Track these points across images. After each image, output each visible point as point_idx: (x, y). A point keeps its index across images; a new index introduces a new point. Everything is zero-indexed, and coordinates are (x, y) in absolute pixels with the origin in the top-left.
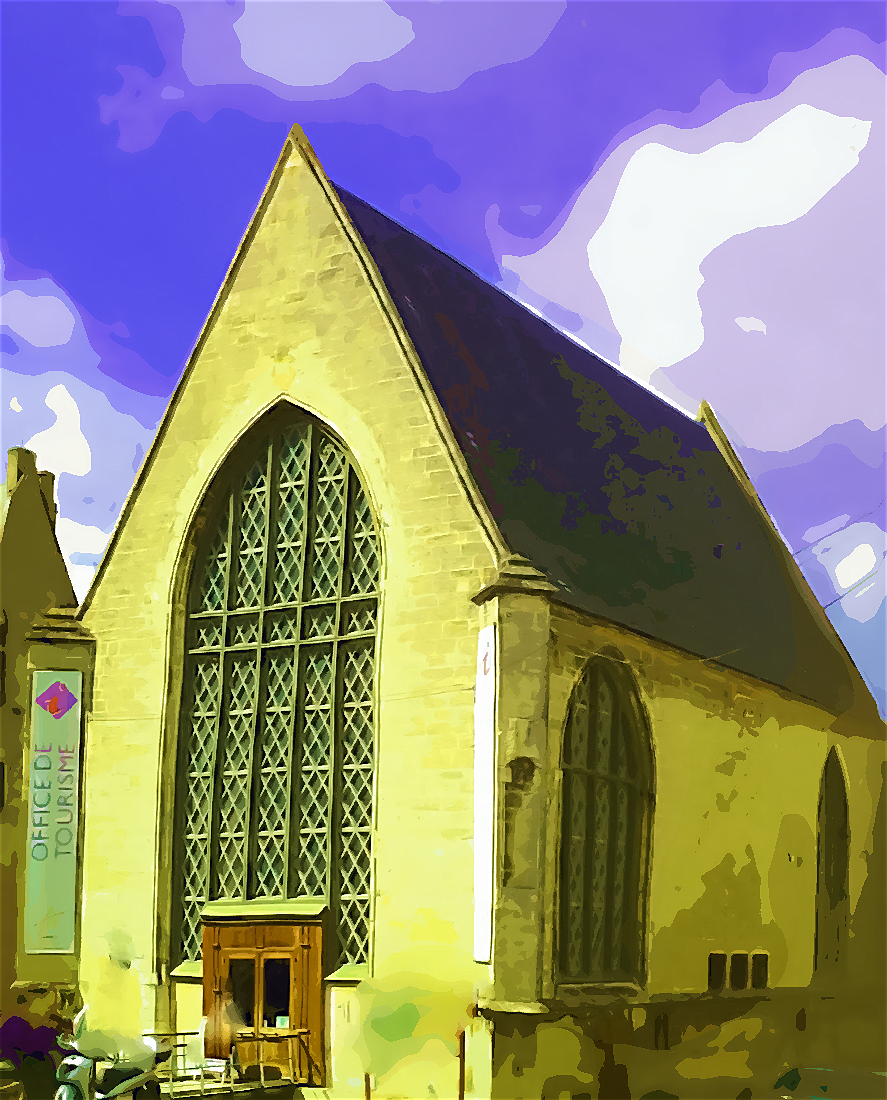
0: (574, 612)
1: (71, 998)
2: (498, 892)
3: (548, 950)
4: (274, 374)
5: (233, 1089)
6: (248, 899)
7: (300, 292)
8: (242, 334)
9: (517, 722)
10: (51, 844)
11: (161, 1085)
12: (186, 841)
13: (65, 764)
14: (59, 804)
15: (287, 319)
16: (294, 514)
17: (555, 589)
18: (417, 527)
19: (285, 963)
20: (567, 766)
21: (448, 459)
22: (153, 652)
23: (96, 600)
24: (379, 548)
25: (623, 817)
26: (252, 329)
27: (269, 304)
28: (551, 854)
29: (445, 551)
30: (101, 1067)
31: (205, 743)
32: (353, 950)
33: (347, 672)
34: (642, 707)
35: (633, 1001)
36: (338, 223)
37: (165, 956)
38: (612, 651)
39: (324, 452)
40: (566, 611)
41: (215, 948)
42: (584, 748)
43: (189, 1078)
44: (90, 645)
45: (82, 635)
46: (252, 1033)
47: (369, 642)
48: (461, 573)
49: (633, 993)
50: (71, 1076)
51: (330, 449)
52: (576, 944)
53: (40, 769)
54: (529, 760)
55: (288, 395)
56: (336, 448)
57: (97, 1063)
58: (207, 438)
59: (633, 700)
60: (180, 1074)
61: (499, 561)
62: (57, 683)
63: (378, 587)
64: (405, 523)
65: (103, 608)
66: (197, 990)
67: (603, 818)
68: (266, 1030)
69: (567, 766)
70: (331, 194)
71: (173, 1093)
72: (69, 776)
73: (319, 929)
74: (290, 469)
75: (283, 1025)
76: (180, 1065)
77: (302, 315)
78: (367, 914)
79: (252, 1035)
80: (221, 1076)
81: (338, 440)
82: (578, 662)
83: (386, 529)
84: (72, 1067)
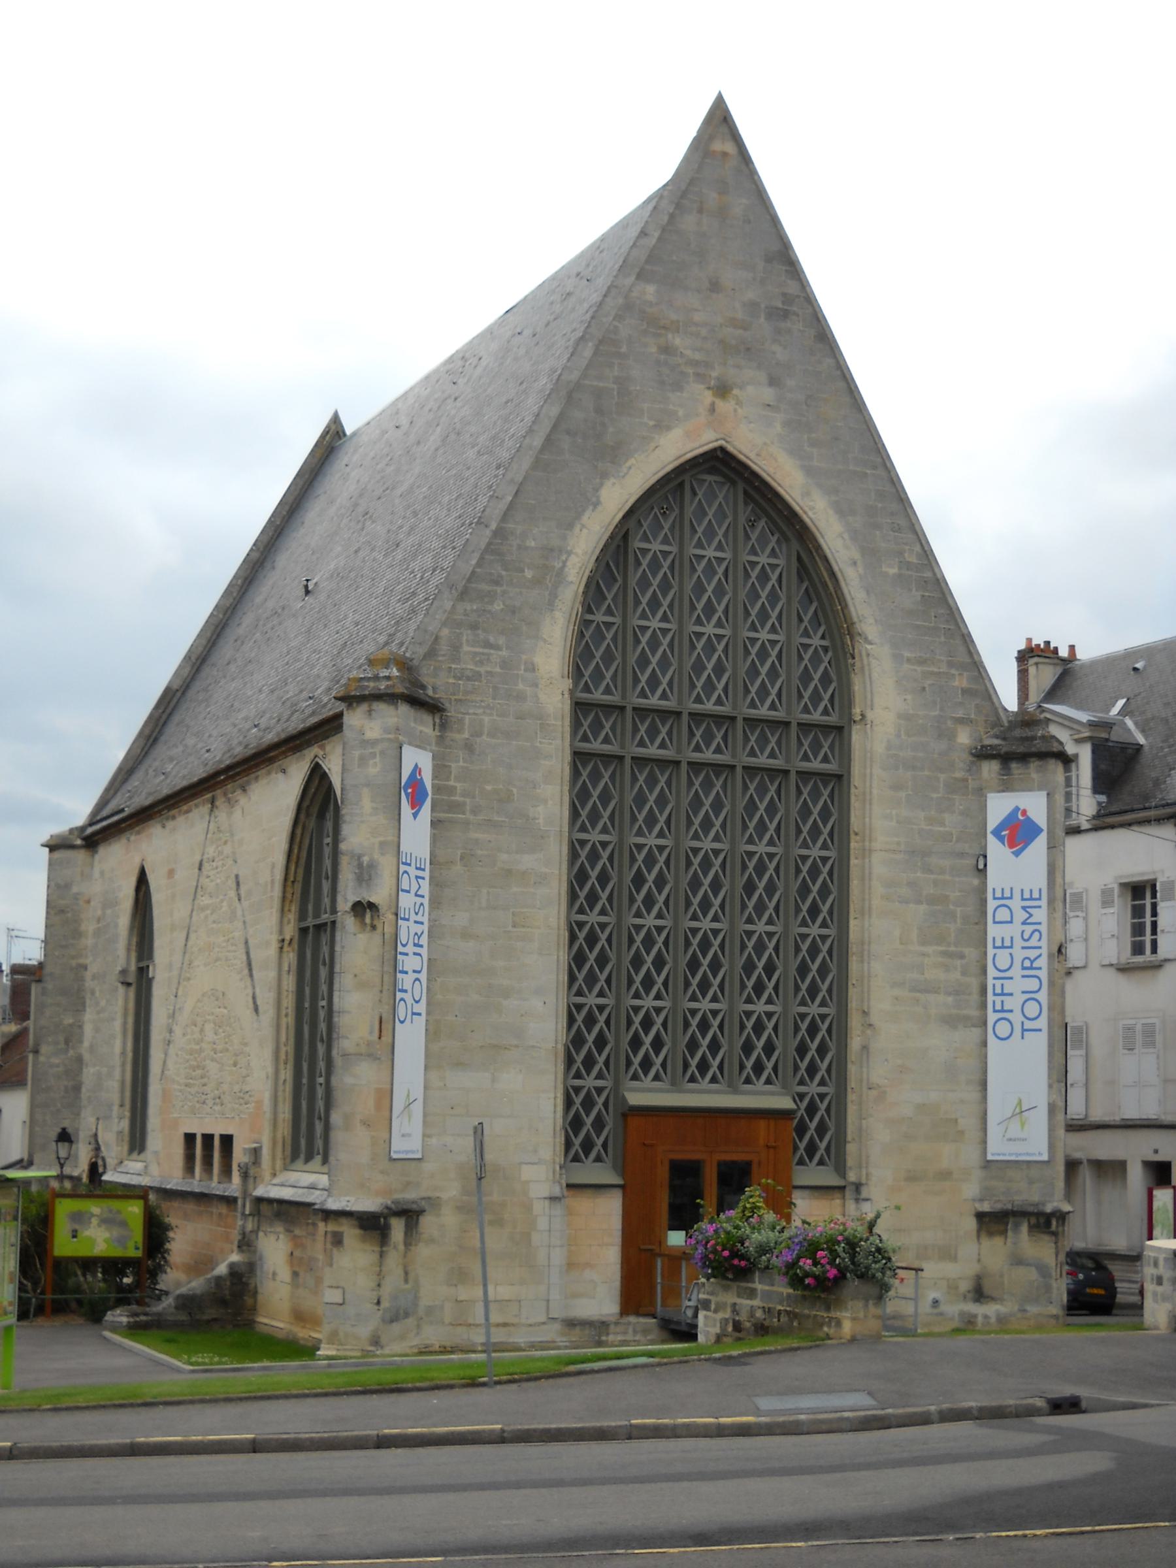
10: (1016, 1017)
13: (1031, 915)
14: (1024, 968)
18: (907, 654)
48: (961, 721)
62: (1017, 809)
72: (1036, 930)
77: (748, 351)
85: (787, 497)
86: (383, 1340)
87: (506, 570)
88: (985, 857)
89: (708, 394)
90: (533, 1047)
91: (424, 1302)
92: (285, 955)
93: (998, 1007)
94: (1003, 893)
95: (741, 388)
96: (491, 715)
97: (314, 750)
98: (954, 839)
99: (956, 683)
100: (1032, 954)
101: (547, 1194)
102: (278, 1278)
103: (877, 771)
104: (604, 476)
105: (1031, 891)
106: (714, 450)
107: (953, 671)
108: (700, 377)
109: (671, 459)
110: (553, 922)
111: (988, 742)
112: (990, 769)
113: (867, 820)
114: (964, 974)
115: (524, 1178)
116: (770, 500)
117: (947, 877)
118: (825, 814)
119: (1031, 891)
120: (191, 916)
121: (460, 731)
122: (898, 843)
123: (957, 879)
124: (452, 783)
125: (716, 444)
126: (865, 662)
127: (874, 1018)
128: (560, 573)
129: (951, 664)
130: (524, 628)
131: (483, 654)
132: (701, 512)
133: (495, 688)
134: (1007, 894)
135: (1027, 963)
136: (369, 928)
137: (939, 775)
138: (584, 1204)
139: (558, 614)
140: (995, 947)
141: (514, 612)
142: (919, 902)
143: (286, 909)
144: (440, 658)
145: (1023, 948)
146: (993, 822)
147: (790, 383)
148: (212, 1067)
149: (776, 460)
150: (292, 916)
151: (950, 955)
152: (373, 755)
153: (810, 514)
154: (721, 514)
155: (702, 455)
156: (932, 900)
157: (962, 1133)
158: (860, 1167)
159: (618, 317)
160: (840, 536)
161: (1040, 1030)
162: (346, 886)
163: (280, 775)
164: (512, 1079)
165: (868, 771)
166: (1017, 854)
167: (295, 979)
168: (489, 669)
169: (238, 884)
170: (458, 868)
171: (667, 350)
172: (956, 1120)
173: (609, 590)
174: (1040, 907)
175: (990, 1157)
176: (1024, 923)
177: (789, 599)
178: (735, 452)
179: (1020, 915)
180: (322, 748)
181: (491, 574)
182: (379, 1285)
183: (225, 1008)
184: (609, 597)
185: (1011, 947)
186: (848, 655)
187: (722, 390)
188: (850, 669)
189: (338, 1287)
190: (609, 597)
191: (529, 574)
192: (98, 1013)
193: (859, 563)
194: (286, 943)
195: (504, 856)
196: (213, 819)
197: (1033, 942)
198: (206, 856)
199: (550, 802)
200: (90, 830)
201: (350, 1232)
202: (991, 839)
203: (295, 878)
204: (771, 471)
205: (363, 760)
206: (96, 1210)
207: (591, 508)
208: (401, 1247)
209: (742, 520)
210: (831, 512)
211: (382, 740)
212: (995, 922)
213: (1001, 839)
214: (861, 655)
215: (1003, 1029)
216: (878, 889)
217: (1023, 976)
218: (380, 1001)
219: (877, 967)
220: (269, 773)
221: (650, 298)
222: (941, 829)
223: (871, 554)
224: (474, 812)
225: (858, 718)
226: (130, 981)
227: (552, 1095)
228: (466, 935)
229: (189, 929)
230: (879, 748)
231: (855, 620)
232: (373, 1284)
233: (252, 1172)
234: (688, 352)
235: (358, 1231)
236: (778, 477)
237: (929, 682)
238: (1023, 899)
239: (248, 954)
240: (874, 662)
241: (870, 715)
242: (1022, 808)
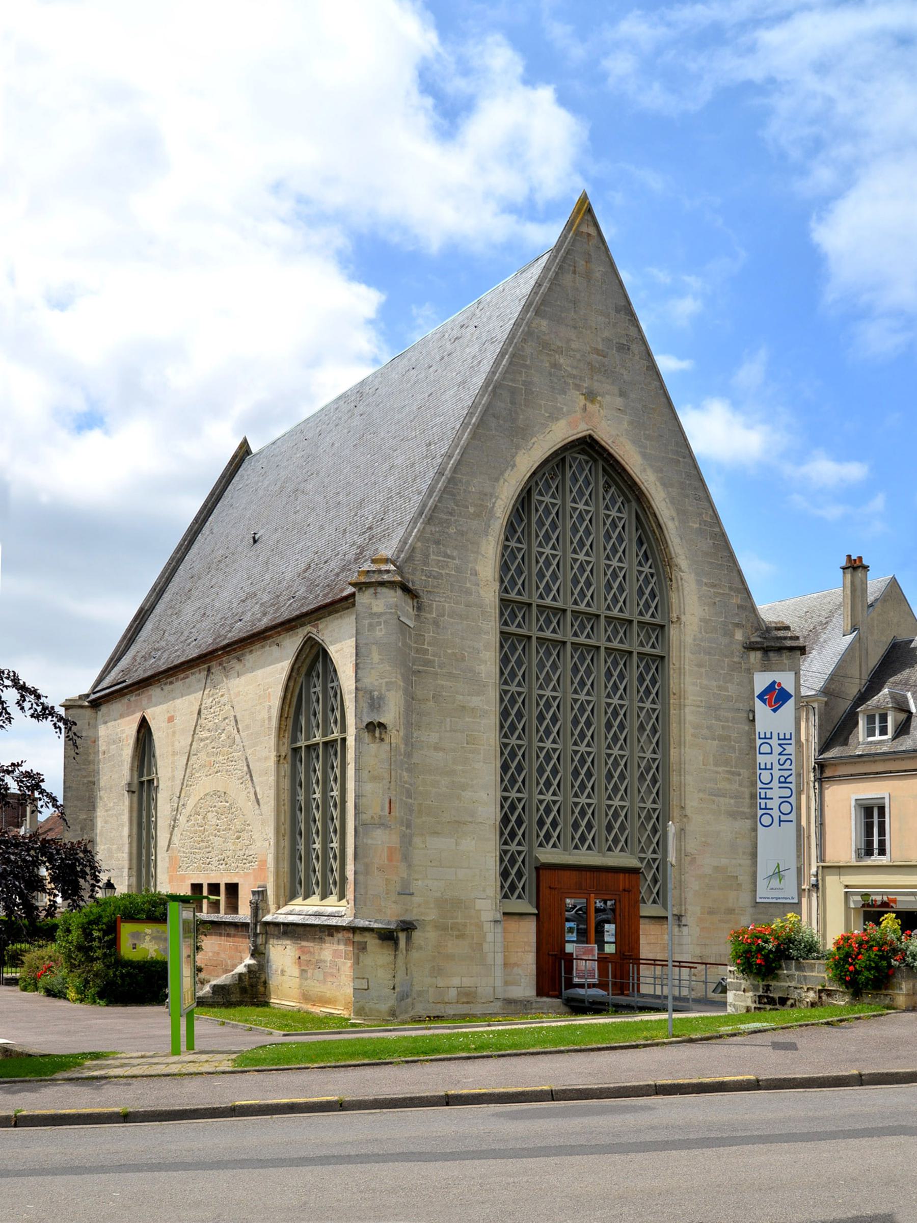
10: (775, 813)
14: (780, 782)
18: (705, 580)
48: (737, 625)
62: (774, 682)
85: (631, 472)
86: (397, 1013)
87: (457, 506)
88: (754, 712)
89: (582, 397)
90: (481, 823)
91: (417, 988)
92: (281, 766)
93: (763, 806)
96: (450, 603)
97: (308, 628)
99: (734, 601)
100: (786, 773)
101: (492, 919)
102: (288, 973)
103: (688, 654)
104: (518, 448)
106: (585, 437)
107: (732, 593)
108: (577, 387)
109: (560, 440)
110: (492, 742)
111: (753, 640)
112: (755, 657)
113: (682, 685)
114: (740, 785)
115: (477, 908)
116: (619, 474)
117: (730, 724)
118: (654, 681)
120: (191, 745)
122: (701, 701)
123: (736, 726)
124: (426, 647)
125: (587, 433)
126: (680, 583)
127: (688, 812)
128: (491, 511)
129: (731, 588)
130: (470, 546)
131: (443, 561)
132: (575, 479)
134: (768, 736)
135: (782, 779)
136: (378, 740)
138: (513, 925)
140: (760, 769)
141: (462, 535)
142: (715, 739)
143: (281, 736)
144: (416, 562)
145: (780, 770)
146: (758, 690)
148: (217, 841)
149: (624, 446)
150: (286, 740)
151: (733, 773)
152: (379, 623)
153: (645, 484)
154: (587, 483)
155: (578, 439)
156: (721, 738)
157: (739, 885)
158: (681, 905)
159: (524, 340)
160: (664, 500)
161: (792, 821)
162: (362, 711)
163: (275, 648)
164: (468, 844)
165: (682, 654)
167: (289, 781)
168: (447, 572)
169: (236, 721)
170: (431, 704)
171: (555, 365)
173: (519, 526)
174: (791, 744)
175: (758, 900)
176: (780, 754)
177: (630, 540)
178: (599, 439)
180: (316, 626)
181: (447, 508)
182: (394, 977)
183: (227, 802)
184: (519, 531)
185: (771, 769)
186: (668, 579)
187: (591, 396)
188: (669, 588)
189: (363, 978)
190: (519, 531)
192: (107, 811)
193: (676, 519)
194: (282, 758)
196: (209, 681)
197: (787, 766)
198: (204, 705)
199: (489, 663)
200: (93, 697)
201: (372, 942)
202: (757, 701)
203: (288, 715)
204: (621, 453)
205: (371, 626)
206: (148, 931)
207: (510, 468)
208: (404, 952)
209: (601, 483)
210: (658, 484)
211: (385, 613)
212: (760, 753)
213: (764, 701)
214: (677, 580)
215: (766, 820)
216: (689, 730)
217: (780, 788)
218: (389, 789)
219: (689, 779)
220: (263, 647)
221: (543, 329)
223: (682, 514)
224: (440, 667)
225: (675, 620)
226: (133, 790)
228: (437, 748)
229: (189, 753)
230: (689, 640)
231: (674, 556)
232: (390, 976)
233: (261, 905)
234: (569, 369)
235: (377, 941)
236: (625, 458)
237: (718, 599)
238: (779, 739)
239: (248, 766)
240: (686, 585)
241: (683, 618)
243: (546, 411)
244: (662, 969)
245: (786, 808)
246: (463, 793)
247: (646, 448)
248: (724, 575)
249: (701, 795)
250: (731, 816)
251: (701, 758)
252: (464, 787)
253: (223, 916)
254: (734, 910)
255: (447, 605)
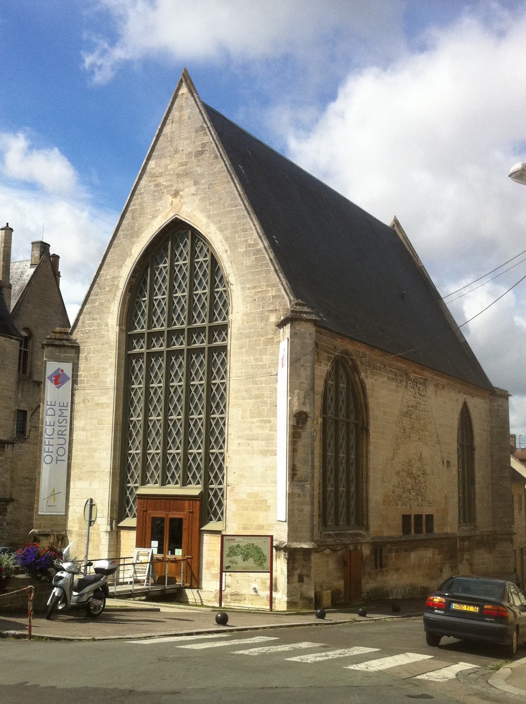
0: (328, 331)
1: (63, 540)
2: (289, 484)
3: (316, 513)
4: (172, 204)
5: (150, 589)
6: (162, 486)
7: (186, 162)
8: (156, 183)
9: (298, 392)
10: (54, 455)
11: (109, 588)
12: (128, 455)
13: (63, 413)
14: (58, 435)
15: (178, 175)
16: (182, 278)
17: (318, 318)
19: (181, 520)
20: (325, 416)
21: (264, 250)
22: (109, 353)
23: (80, 323)
24: (228, 297)
25: (353, 442)
26: (161, 180)
27: (169, 168)
28: (317, 463)
29: (263, 299)
30: (76, 577)
31: (138, 402)
32: (215, 514)
33: (211, 364)
34: (362, 382)
35: (362, 540)
36: (205, 126)
37: (115, 516)
38: (347, 353)
39: (198, 246)
40: (323, 331)
41: (144, 511)
42: (333, 405)
43: (126, 583)
44: (76, 348)
45: (72, 343)
46: (162, 557)
47: (224, 348)
48: (271, 311)
49: (363, 536)
50: (61, 582)
51: (200, 244)
52: (331, 510)
53: (55, 414)
54: (305, 413)
55: (178, 215)
56: (204, 244)
57: (75, 576)
58: (137, 237)
59: (357, 378)
60: (121, 580)
61: (290, 304)
62: (59, 369)
63: (228, 318)
64: (242, 283)
65: (83, 328)
66: (133, 535)
67: (343, 442)
68: (169, 556)
69: (325, 416)
70: (202, 109)
71: (134, 590)
73: (198, 502)
74: (180, 255)
75: (179, 552)
76: (121, 576)
77: (186, 174)
78: (223, 496)
79: (162, 559)
80: (144, 582)
81: (204, 240)
82: (329, 359)
83: (231, 286)
84: (61, 578)
90: (103, 471)
94: (63, 404)
95: (183, 191)
98: (267, 367)
99: (270, 294)
100: (63, 429)
101: (105, 530)
105: (51, 402)
107: (269, 289)
117: (264, 385)
119: (51, 402)
121: (84, 353)
122: (242, 373)
123: (268, 386)
131: (92, 323)
133: (95, 335)
134: (53, 404)
135: (60, 433)
137: (261, 338)
139: (116, 302)
141: (102, 305)
147: (203, 181)
161: (64, 460)
164: (96, 485)
166: (58, 388)
168: (93, 328)
170: (82, 404)
172: (266, 500)
174: (67, 410)
176: (60, 416)
179: (58, 413)
185: (54, 426)
191: (107, 289)
195: (96, 398)
197: (63, 424)
199: (111, 375)
204: (193, 222)
207: (129, 257)
210: (217, 232)
217: (58, 438)
222: (262, 363)
223: (233, 246)
227: (108, 490)
228: (83, 430)
234: (165, 183)
238: (60, 406)
242: (62, 369)
243: (150, 215)
244: (124, 567)
245: (61, 451)
246: (95, 454)
247: (209, 211)
248: (263, 277)
249: (240, 441)
250: (262, 454)
251: (240, 413)
252: (95, 450)
253: (423, 536)
254: (263, 526)
255: (92, 347)
